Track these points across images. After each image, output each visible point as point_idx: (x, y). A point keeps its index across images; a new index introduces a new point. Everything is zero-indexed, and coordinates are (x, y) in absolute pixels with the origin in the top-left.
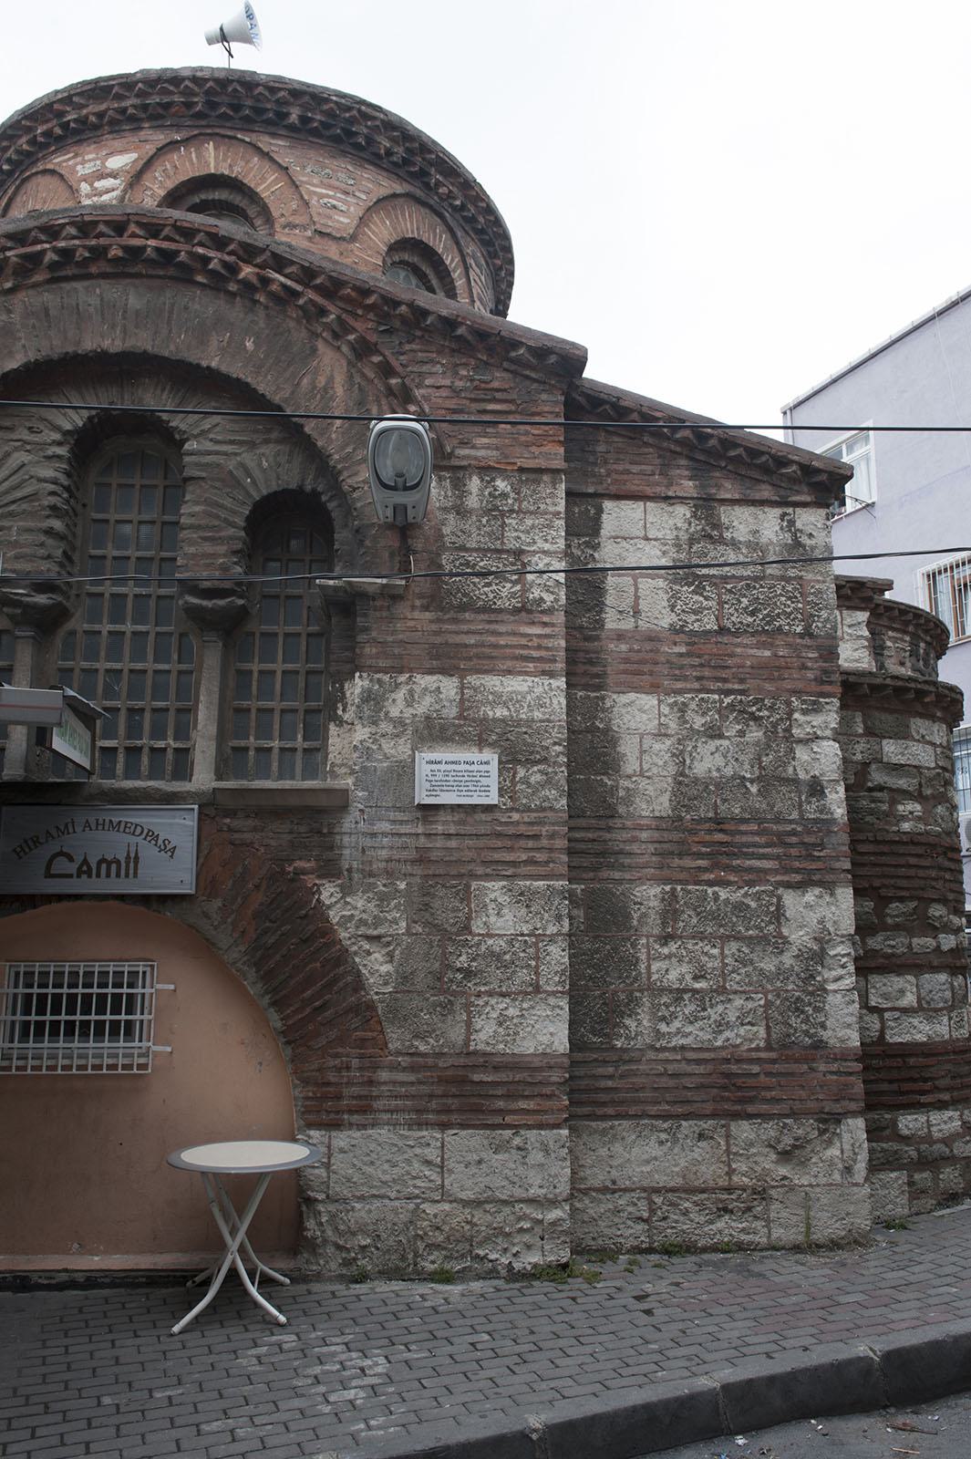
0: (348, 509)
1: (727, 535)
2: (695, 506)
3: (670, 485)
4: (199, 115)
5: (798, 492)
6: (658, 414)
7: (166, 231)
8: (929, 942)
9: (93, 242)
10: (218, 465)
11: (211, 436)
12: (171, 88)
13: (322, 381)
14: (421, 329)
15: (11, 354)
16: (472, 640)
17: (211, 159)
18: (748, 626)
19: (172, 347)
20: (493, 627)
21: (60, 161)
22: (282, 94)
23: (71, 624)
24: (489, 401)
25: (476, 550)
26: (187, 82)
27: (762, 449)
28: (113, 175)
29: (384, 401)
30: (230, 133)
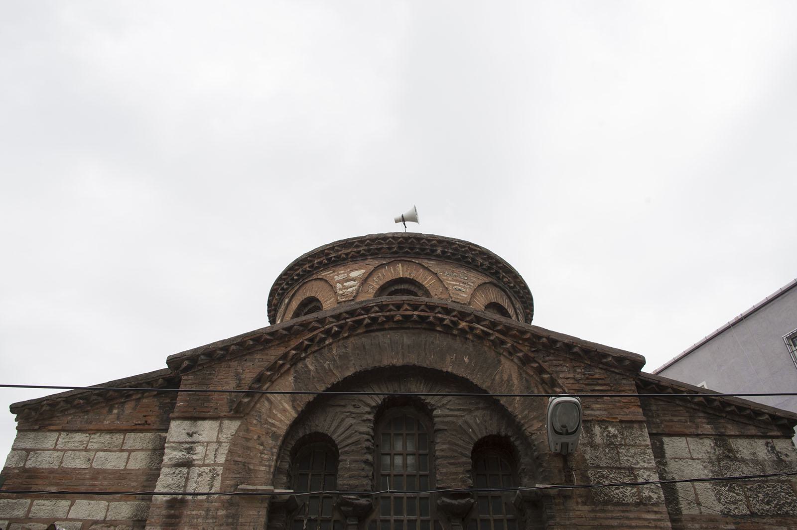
0: (528, 443)
1: (738, 456)
2: (715, 439)
3: (697, 427)
4: (396, 253)
5: (772, 430)
6: (683, 389)
7: (422, 307)
9: (388, 314)
10: (453, 422)
11: (448, 407)
12: (382, 242)
13: (505, 377)
14: (553, 349)
15: (348, 368)
16: (615, 523)
17: (400, 271)
18: (768, 511)
19: (428, 362)
20: (627, 514)
21: (324, 274)
22: (434, 242)
23: (373, 516)
24: (595, 385)
25: (607, 468)
26: (390, 239)
27: (745, 406)
28: (354, 280)
29: (540, 387)
30: (409, 259)
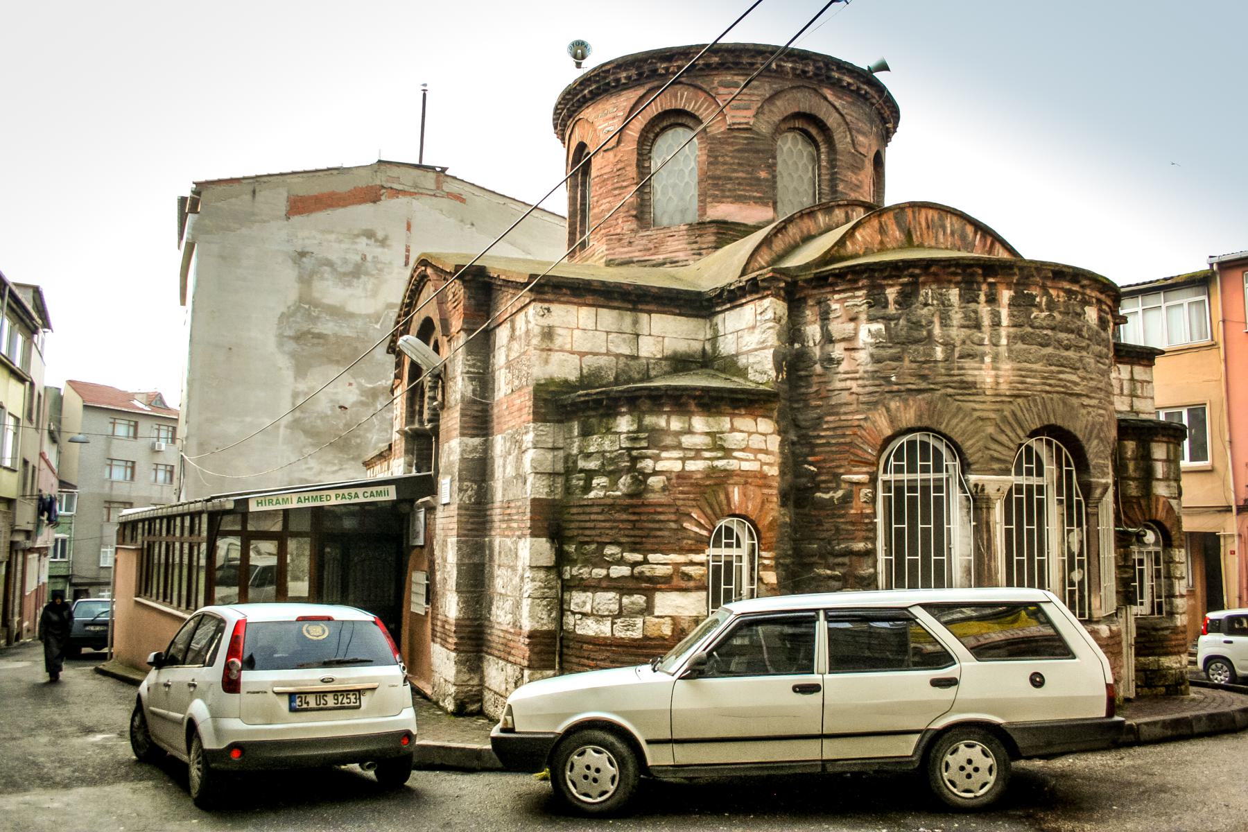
8: (603, 572)
